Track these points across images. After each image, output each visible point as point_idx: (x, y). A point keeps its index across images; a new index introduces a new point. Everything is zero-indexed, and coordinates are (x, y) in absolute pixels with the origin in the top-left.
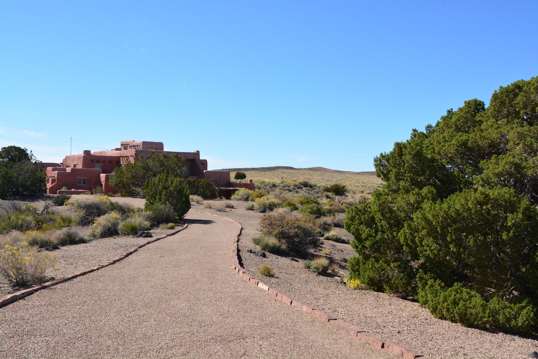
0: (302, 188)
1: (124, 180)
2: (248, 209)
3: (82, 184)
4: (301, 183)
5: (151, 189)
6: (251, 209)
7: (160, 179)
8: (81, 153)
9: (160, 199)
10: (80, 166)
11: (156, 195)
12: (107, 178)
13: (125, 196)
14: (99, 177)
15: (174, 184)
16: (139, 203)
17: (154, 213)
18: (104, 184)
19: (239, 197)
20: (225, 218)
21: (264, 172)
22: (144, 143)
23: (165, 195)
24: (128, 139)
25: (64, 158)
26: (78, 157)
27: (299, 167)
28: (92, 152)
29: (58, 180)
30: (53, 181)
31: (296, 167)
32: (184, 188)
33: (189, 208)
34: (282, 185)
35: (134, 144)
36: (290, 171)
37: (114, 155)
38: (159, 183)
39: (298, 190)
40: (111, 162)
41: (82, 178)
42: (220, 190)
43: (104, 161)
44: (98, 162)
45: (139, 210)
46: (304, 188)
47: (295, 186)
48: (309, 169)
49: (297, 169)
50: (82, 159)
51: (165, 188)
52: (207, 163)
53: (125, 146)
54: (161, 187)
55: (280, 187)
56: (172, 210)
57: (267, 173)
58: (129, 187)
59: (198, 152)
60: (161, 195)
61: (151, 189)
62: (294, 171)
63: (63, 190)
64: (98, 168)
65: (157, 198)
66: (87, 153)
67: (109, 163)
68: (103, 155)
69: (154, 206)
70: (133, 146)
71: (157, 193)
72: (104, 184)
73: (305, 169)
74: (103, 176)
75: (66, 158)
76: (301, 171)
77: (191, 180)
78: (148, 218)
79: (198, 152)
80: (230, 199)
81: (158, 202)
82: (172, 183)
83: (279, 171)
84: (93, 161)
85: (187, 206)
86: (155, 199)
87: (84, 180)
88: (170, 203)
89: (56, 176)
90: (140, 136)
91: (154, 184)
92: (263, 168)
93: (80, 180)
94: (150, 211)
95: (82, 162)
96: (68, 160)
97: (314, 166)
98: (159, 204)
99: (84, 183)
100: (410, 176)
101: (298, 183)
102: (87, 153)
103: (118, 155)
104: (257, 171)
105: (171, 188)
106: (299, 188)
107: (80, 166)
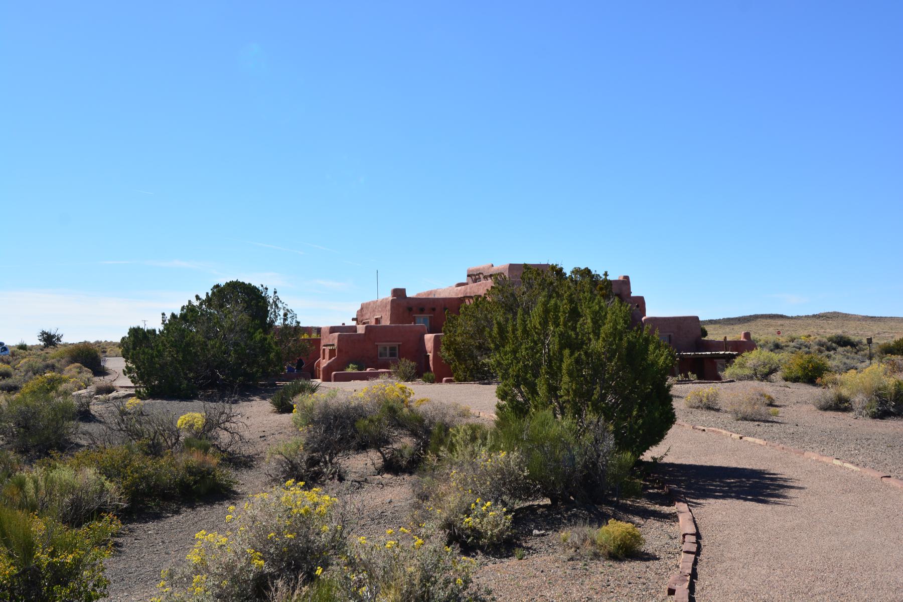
0: (835, 349)
1: (459, 339)
2: (826, 408)
3: (388, 357)
4: (830, 339)
5: (514, 352)
6: (840, 405)
7: (546, 311)
8: (387, 295)
9: (553, 390)
10: (386, 322)
11: (536, 375)
12: (437, 341)
13: (465, 380)
15: (606, 328)
16: (480, 402)
17: (528, 453)
18: (431, 355)
19: (747, 372)
20: (814, 456)
21: (732, 327)
22: (512, 267)
23: (570, 374)
24: (479, 263)
25: (359, 308)
26: (383, 303)
27: (794, 315)
28: (409, 294)
29: (339, 351)
30: (332, 353)
31: (790, 315)
32: (647, 341)
33: (669, 419)
34: (792, 344)
35: (492, 271)
36: (780, 322)
37: (454, 296)
38: (544, 323)
39: (827, 353)
41: (388, 345)
42: (682, 357)
43: (434, 309)
44: (422, 311)
45: (475, 434)
46: (840, 349)
47: (821, 344)
48: (814, 316)
49: (792, 318)
50: (389, 307)
51: (569, 343)
52: (644, 303)
53: (474, 276)
54: (553, 342)
55: (789, 349)
56: (610, 442)
58: (473, 357)
59: (627, 278)
60: (554, 373)
61: (514, 352)
62: (787, 322)
63: (349, 370)
65: (542, 390)
66: (399, 293)
67: (436, 311)
68: (431, 296)
69: (530, 425)
70: (491, 276)
71: (537, 365)
72: (431, 355)
73: (807, 317)
74: (429, 338)
75: (362, 309)
76: (799, 321)
78: (507, 486)
79: (627, 278)
80: (718, 378)
81: (545, 406)
82: (598, 320)
83: (759, 322)
84: (410, 309)
85: (661, 421)
86: (533, 391)
88: (596, 409)
89: (336, 342)
90: (501, 257)
91: (525, 331)
92: (729, 319)
93: (385, 348)
94: (510, 450)
95: (389, 314)
96: (365, 311)
97: (823, 312)
98: (548, 413)
101: (825, 340)
102: (399, 293)
104: (717, 326)
105: (597, 345)
106: (829, 349)
107: (386, 322)
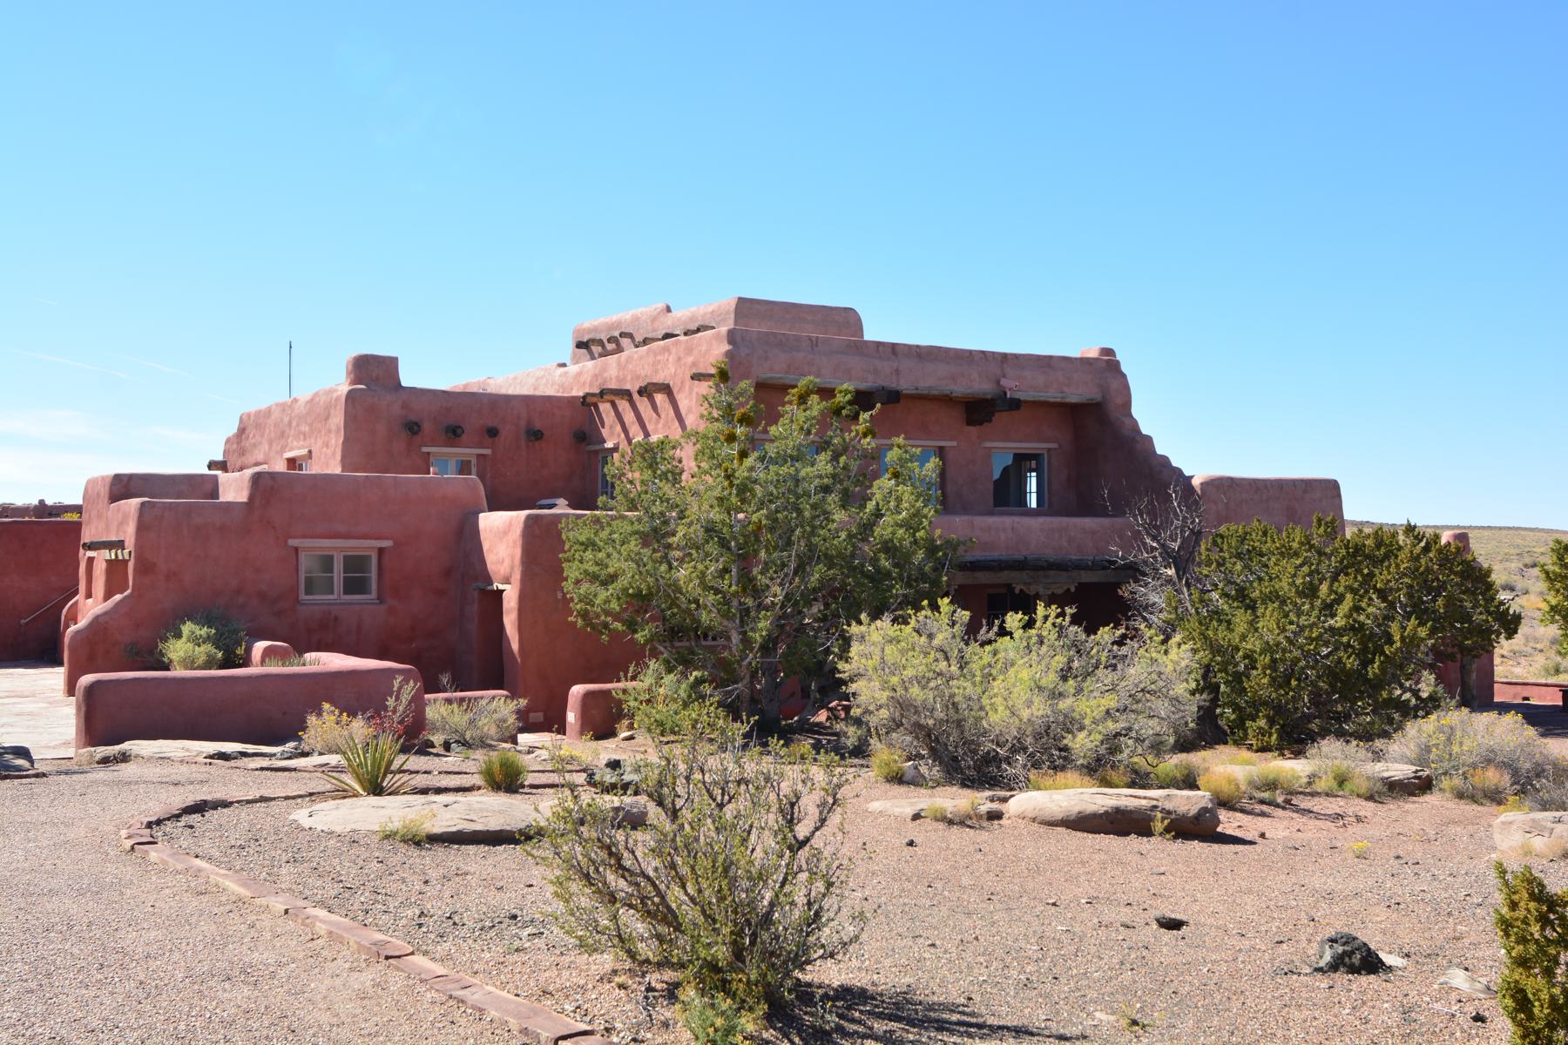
3: (338, 595)
8: (339, 382)
10: (328, 461)
12: (542, 547)
14: (467, 536)
26: (316, 411)
29: (144, 567)
37: (551, 392)
40: (535, 435)
41: (340, 548)
43: (493, 432)
44: (453, 434)
50: (338, 419)
57: (472, 849)
64: (447, 474)
66: (374, 372)
74: (501, 534)
77: (809, 469)
84: (413, 428)
87: (355, 564)
89: (129, 534)
93: (327, 563)
95: (336, 441)
96: (251, 432)
99: (355, 585)
100: (1411, 587)
102: (374, 372)
103: (578, 392)
107: (328, 461)
